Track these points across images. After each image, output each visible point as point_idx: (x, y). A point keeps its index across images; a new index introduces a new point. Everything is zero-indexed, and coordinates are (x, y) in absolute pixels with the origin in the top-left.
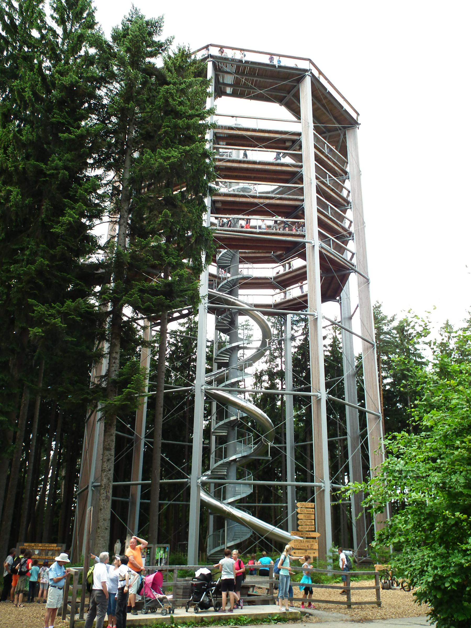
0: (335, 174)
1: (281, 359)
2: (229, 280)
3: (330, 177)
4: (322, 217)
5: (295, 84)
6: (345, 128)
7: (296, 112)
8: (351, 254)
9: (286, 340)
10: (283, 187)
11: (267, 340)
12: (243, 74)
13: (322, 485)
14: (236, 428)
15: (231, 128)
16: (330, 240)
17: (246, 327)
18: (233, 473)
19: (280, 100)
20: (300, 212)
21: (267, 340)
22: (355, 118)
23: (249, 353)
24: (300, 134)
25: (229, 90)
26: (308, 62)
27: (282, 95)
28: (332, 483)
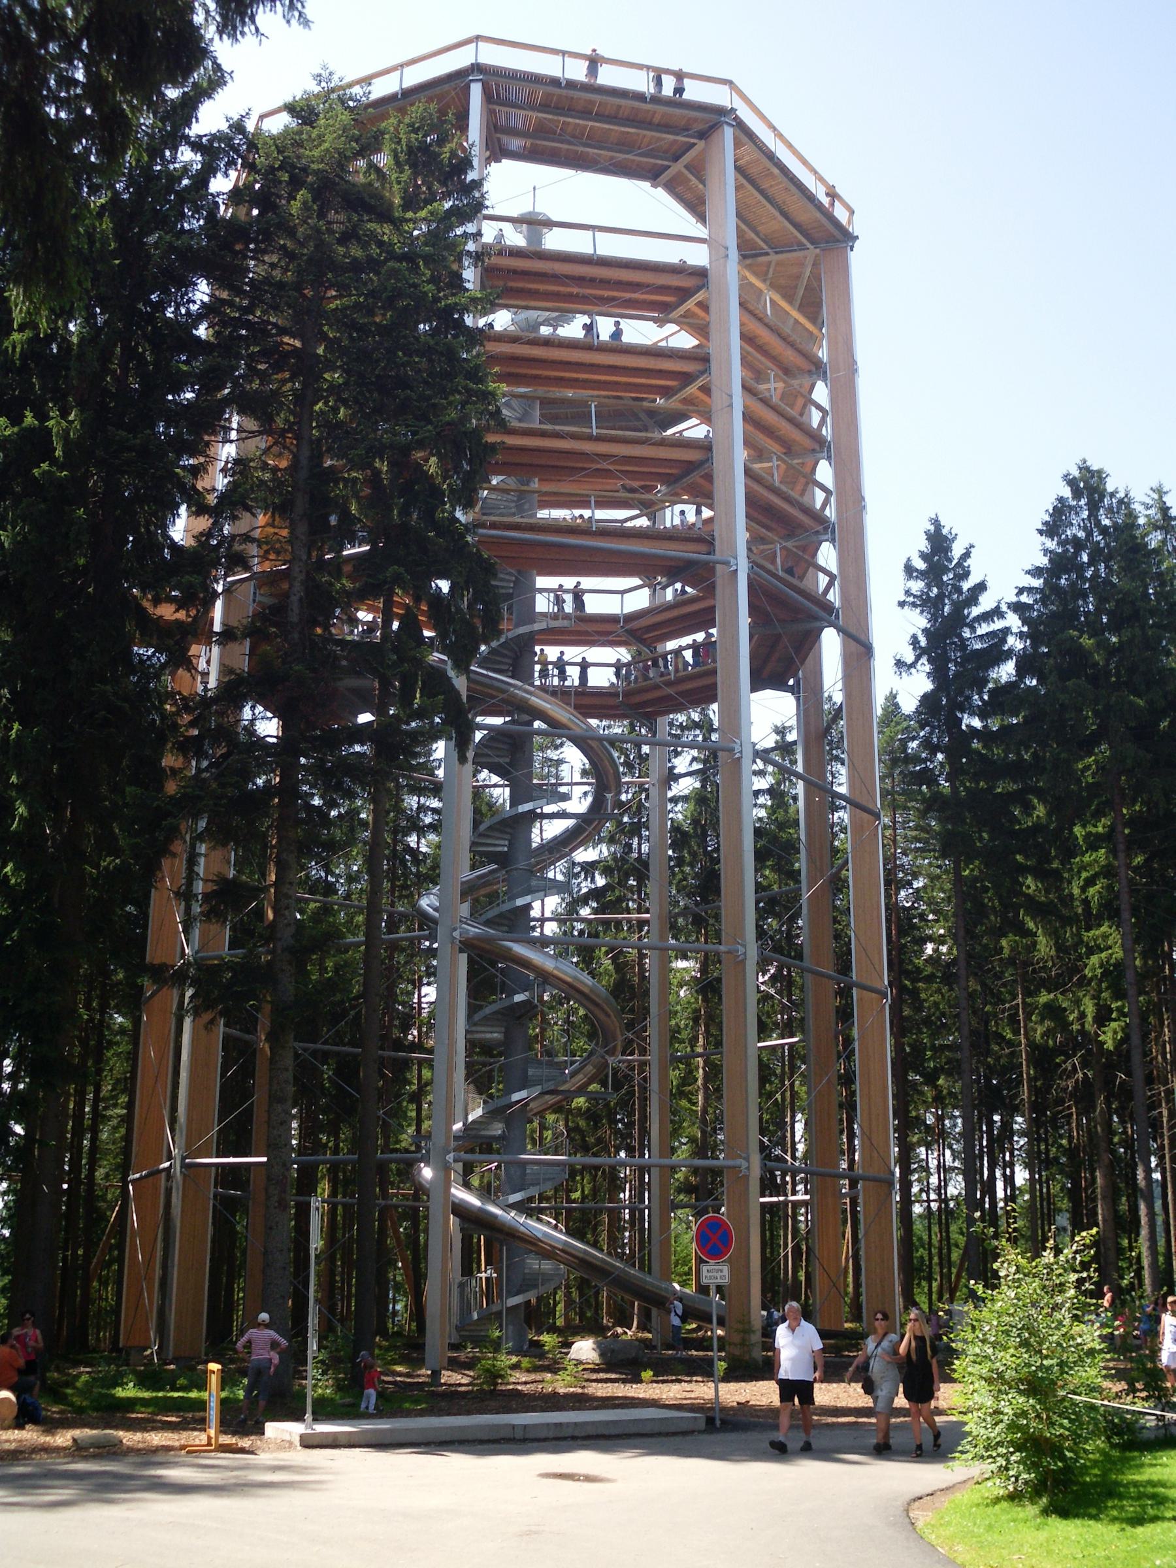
5: (693, 141)
7: (697, 207)
15: (527, 308)
24: (701, 274)
25: (516, 144)
26: (726, 88)
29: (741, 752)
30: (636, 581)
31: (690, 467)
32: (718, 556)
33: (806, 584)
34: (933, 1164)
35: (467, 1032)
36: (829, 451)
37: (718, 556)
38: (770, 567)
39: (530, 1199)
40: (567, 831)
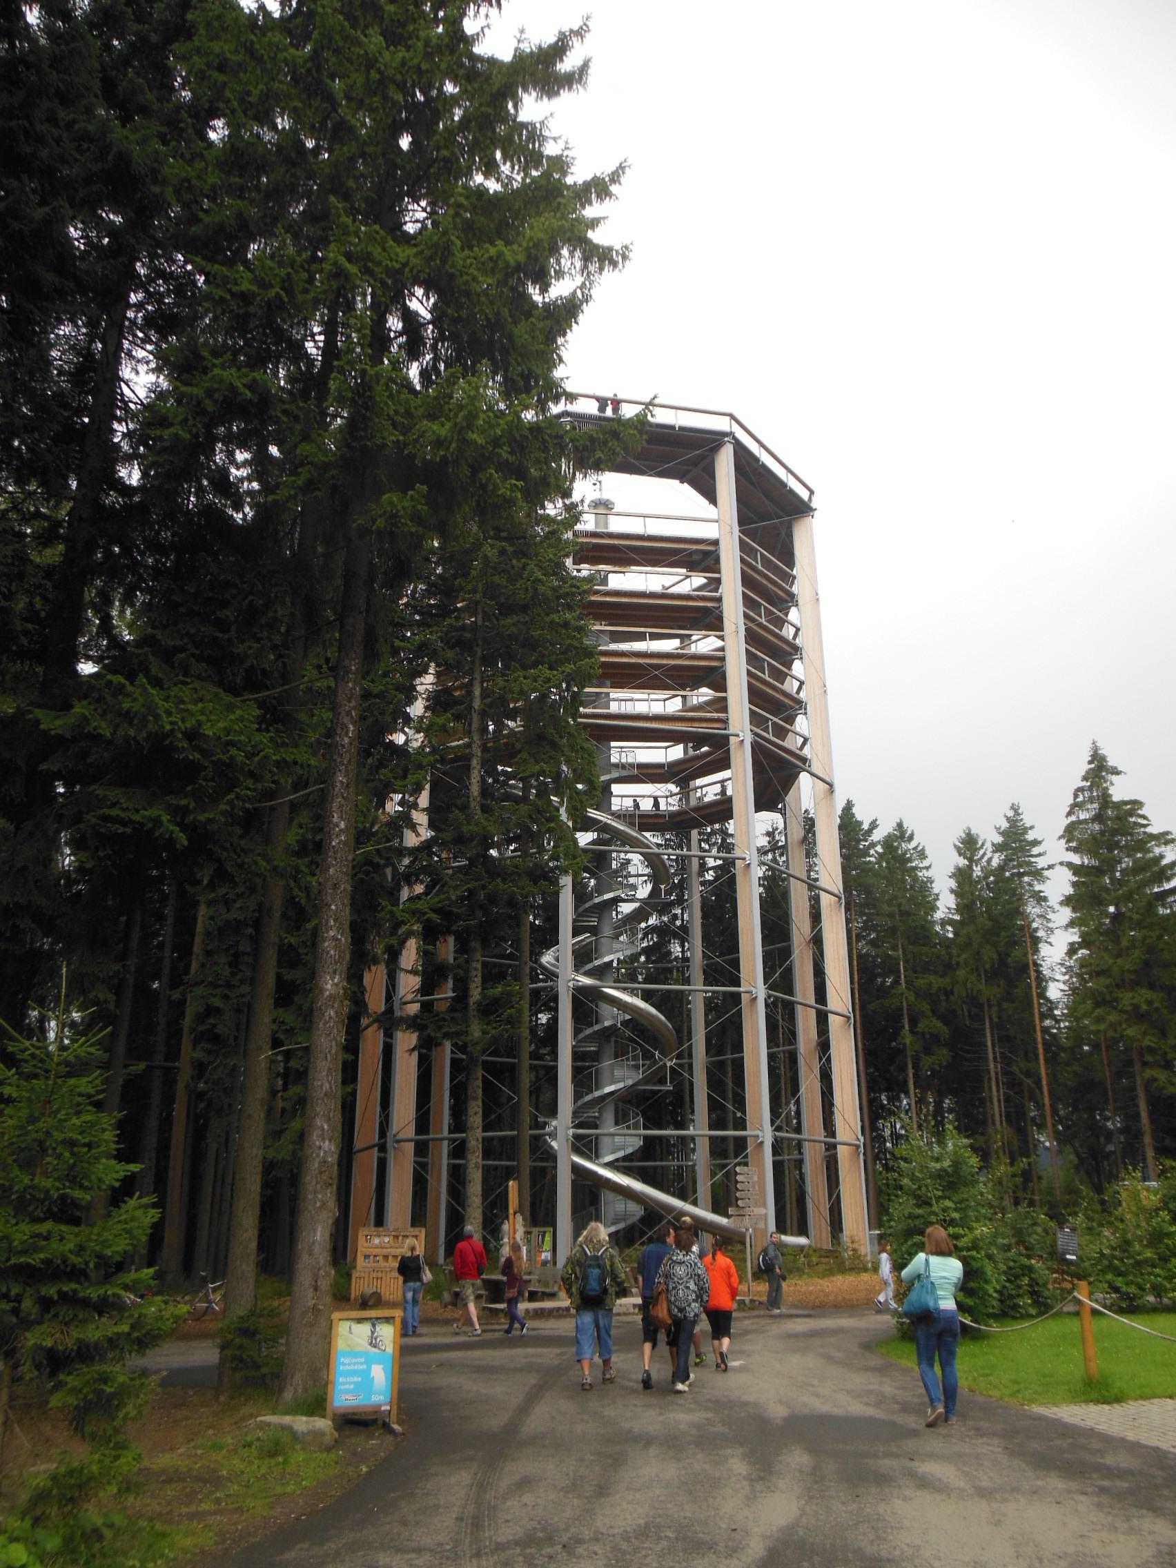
4: (754, 682)
13: (760, 1133)
18: (609, 1116)
19: (681, 475)
24: (716, 543)
26: (728, 418)
31: (706, 554)
32: (731, 730)
33: (784, 633)
34: (887, 1133)
37: (731, 730)
38: (765, 734)
39: (617, 1160)
40: (635, 910)
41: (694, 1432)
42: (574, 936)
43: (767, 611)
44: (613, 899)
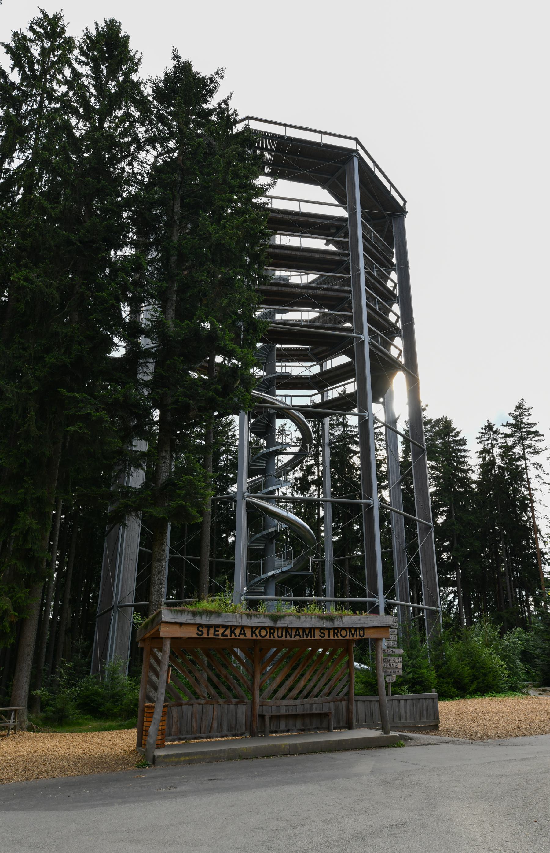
0: (382, 265)
1: (318, 467)
2: (265, 378)
3: (377, 267)
5: (340, 165)
6: (390, 216)
8: (399, 352)
9: (324, 446)
10: (328, 276)
11: (308, 445)
12: (283, 152)
14: (274, 541)
16: (377, 336)
17: (282, 431)
18: (272, 589)
19: (323, 184)
20: (346, 305)
21: (308, 445)
22: (402, 205)
23: (284, 459)
26: (354, 142)
27: (326, 176)
28: (386, 598)
29: (368, 417)
30: (316, 392)
35: (248, 546)
36: (398, 300)
41: (485, 694)
42: (250, 476)
43: (378, 271)
44: (275, 451)
